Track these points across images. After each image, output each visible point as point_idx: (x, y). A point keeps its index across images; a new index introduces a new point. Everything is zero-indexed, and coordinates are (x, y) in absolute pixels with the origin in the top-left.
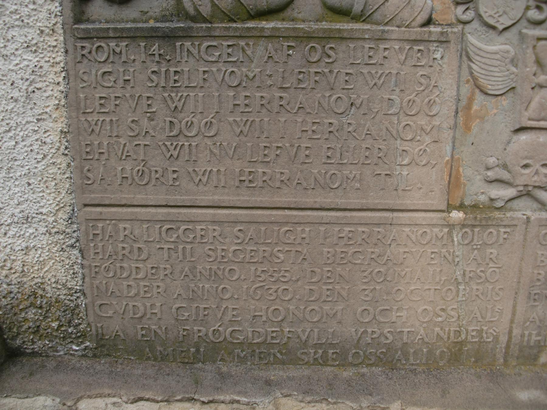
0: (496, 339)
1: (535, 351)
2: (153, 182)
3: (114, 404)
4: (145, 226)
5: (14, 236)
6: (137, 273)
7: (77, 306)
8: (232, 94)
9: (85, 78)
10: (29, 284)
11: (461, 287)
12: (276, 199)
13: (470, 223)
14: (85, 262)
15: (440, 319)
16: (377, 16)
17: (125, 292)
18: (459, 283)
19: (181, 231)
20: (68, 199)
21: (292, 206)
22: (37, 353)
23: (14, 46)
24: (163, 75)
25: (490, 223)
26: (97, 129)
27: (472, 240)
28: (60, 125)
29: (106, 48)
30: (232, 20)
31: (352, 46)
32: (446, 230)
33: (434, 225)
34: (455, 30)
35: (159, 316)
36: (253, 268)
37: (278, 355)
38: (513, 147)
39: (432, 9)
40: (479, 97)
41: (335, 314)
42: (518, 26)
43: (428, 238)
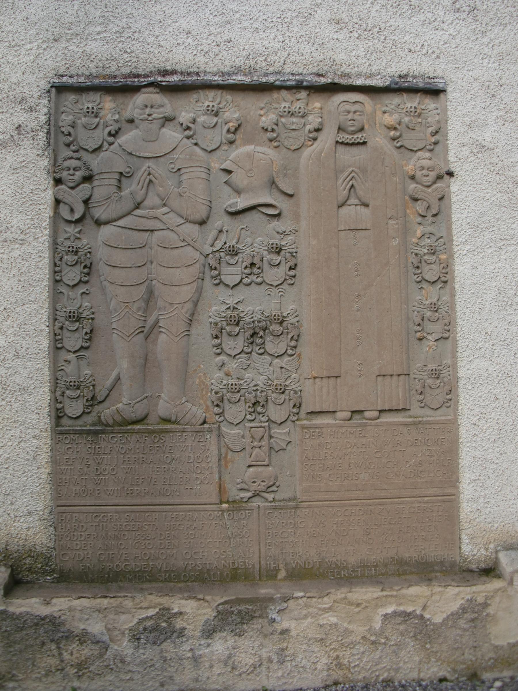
0: (253, 566)
1: (275, 573)
2: (89, 495)
3: (69, 600)
4: (85, 515)
5: (23, 522)
6: (81, 538)
7: (51, 556)
8: (122, 456)
9: (60, 450)
10: (28, 545)
11: (232, 540)
12: (143, 501)
13: (231, 509)
14: (57, 533)
15: (224, 556)
16: (182, 422)
17: (75, 547)
18: (230, 538)
19: (101, 517)
20: (51, 504)
21: (150, 504)
22: (29, 581)
23: (29, 437)
24: (93, 449)
25: (241, 509)
26: (65, 472)
27: (233, 517)
28: (47, 471)
29: (69, 438)
30: (121, 426)
31: (171, 435)
32: (220, 513)
33: (215, 511)
34: (215, 426)
35: (91, 558)
36: (134, 533)
37: (148, 577)
38: (247, 474)
39: (206, 417)
40: (230, 453)
41: (173, 555)
42: (243, 422)
43: (212, 517)
